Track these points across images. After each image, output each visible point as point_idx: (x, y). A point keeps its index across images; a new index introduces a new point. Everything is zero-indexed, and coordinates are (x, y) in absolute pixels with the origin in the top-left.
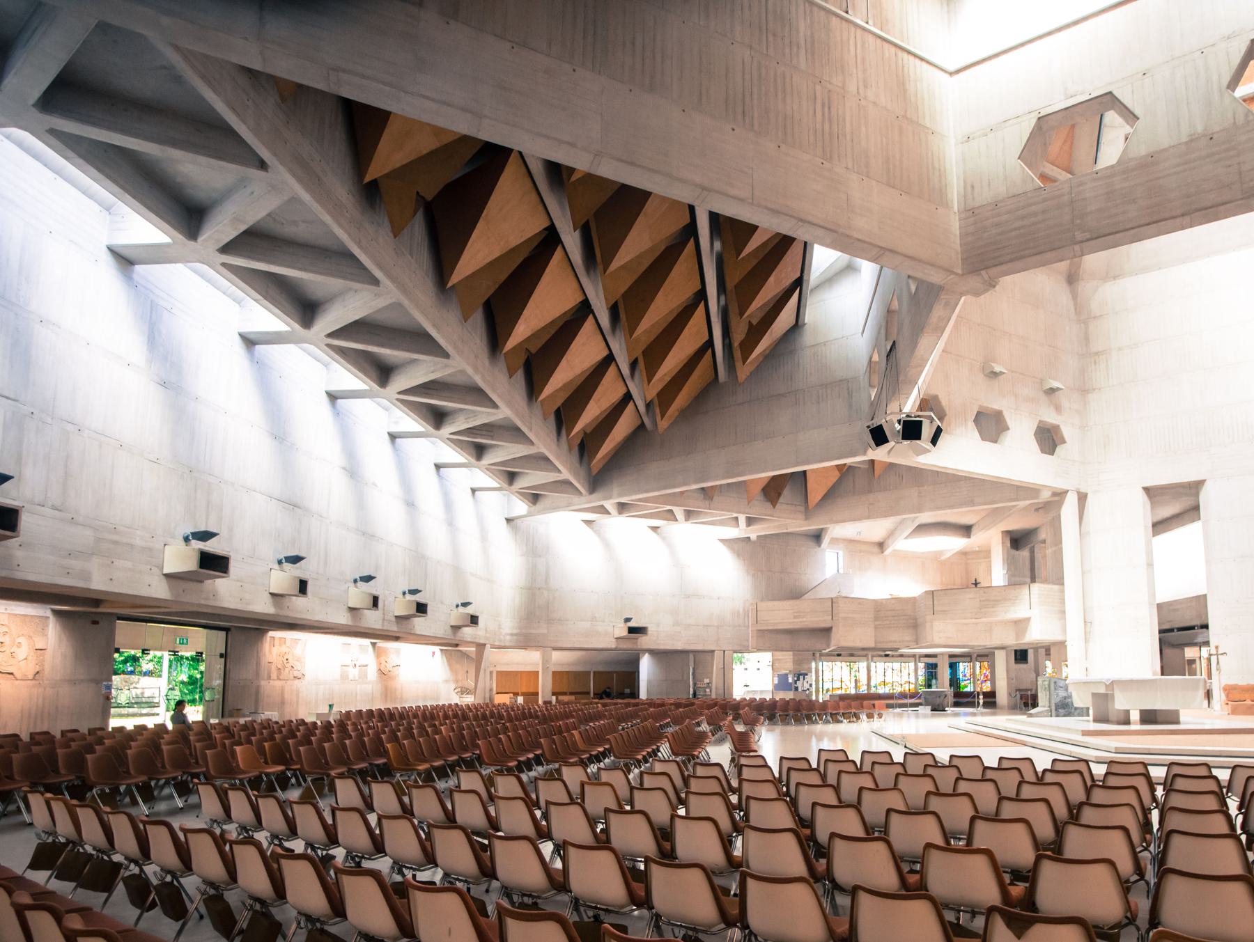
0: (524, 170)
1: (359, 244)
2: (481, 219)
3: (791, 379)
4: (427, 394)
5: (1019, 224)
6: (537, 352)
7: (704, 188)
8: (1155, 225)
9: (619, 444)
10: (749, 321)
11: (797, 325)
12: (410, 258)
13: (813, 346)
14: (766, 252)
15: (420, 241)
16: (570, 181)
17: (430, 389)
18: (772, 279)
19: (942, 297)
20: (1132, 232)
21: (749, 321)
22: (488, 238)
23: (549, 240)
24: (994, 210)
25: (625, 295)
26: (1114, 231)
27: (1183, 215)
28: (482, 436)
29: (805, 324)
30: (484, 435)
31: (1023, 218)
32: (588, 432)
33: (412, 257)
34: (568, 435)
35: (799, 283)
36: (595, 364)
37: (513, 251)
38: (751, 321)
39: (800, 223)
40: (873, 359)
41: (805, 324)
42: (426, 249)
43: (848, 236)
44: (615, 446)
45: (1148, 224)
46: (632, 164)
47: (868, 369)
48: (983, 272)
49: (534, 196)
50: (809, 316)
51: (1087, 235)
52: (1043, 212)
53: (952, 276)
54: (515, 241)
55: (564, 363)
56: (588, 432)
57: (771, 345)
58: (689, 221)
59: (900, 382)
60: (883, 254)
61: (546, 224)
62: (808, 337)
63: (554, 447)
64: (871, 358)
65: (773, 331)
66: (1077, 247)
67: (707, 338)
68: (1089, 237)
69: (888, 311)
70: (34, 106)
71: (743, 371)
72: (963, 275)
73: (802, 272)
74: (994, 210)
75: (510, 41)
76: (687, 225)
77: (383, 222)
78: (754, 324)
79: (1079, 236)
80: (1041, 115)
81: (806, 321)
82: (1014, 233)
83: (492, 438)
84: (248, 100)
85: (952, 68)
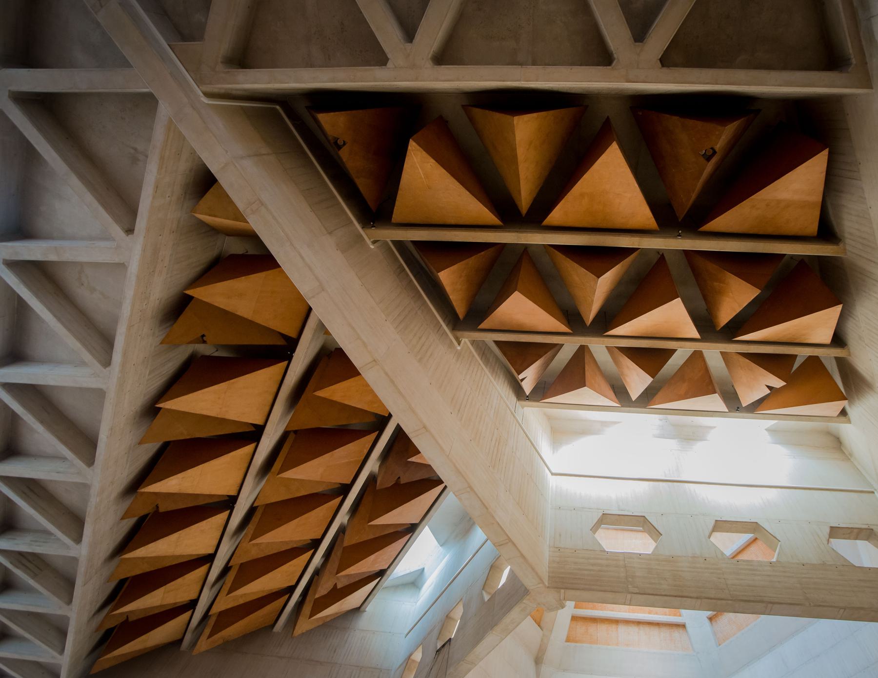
0: (280, 378)
1: (130, 327)
2: (228, 382)
3: (335, 651)
4: (25, 493)
5: (591, 568)
6: (164, 512)
7: (425, 427)
8: (680, 598)
9: (145, 649)
10: (336, 584)
11: (357, 610)
12: (148, 373)
13: (363, 630)
14: (382, 534)
15: (164, 373)
16: (314, 393)
17: (31, 490)
18: (372, 557)
19: (524, 601)
20: (666, 598)
21: (336, 584)
22: (219, 398)
23: (254, 434)
24: (573, 553)
25: (268, 506)
26: (654, 593)
27: (697, 598)
28: (26, 568)
29: (366, 611)
30: (29, 569)
31: (593, 565)
32: (130, 619)
33: (149, 375)
34: (113, 610)
35: (381, 573)
36: (198, 555)
37: (223, 421)
38: (337, 584)
39: (468, 489)
40: (413, 657)
41: (366, 611)
42: (162, 381)
43: (493, 516)
44: (140, 650)
45: (676, 596)
46: (392, 382)
47: (405, 664)
48: (562, 591)
49: (270, 399)
50: (370, 608)
51: (636, 590)
52: (607, 566)
53: (541, 585)
54: (232, 415)
55: (174, 537)
56: (130, 619)
57: (337, 613)
58: (349, 483)
59: (447, 674)
60: (507, 543)
61: (259, 421)
62: (364, 622)
63: (85, 618)
64: (411, 655)
65: (345, 602)
66: (629, 596)
67: (293, 583)
68: (638, 591)
69: (447, 616)
70: (9, 91)
71: (304, 625)
72: (548, 587)
73: (389, 567)
74: (573, 553)
75: (362, 282)
76: (347, 484)
77: (157, 337)
78: (338, 588)
79: (631, 589)
80: (604, 513)
81: (367, 609)
82: (586, 572)
83: (34, 576)
84: (169, 197)
85: (553, 471)
